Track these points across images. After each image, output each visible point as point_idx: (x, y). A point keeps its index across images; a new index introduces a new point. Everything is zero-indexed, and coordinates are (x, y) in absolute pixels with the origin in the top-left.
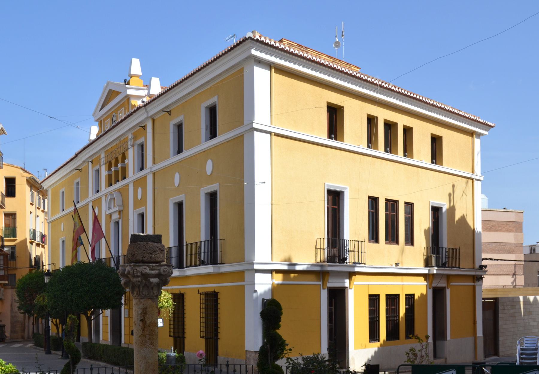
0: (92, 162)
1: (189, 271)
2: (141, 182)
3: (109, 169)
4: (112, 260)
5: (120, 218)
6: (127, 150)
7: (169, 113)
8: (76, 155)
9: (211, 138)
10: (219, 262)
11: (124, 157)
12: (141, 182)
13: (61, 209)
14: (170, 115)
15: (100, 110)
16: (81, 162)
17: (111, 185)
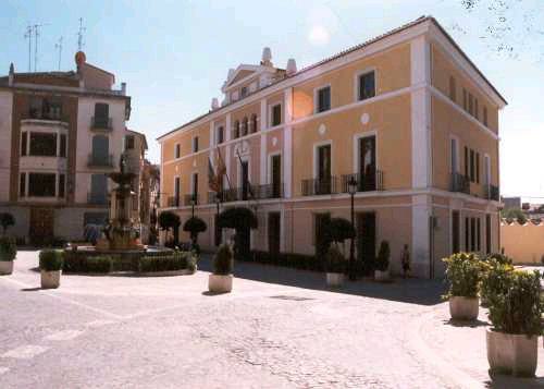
9: (321, 111)
17: (238, 136)
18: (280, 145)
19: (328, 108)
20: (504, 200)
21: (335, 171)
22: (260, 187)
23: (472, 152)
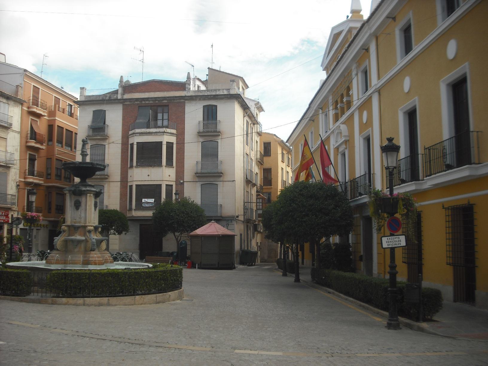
0: (322, 109)
1: (428, 183)
2: (366, 105)
3: (336, 108)
5: (346, 148)
8: (310, 105)
11: (349, 89)
12: (366, 105)
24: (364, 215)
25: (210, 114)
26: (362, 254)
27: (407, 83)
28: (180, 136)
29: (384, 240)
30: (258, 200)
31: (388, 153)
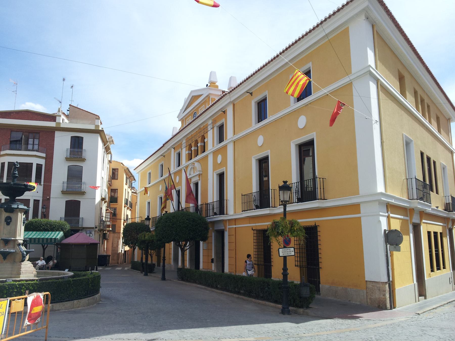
0: (174, 148)
4: (204, 205)
6: (207, 132)
7: (251, 94)
8: (164, 145)
9: (258, 122)
10: (271, 206)
11: (203, 138)
13: (148, 183)
14: (252, 95)
15: (202, 95)
16: (166, 149)
18: (224, 162)
19: (265, 117)
20: (443, 231)
21: (274, 183)
22: (207, 204)
23: (429, 159)
24: (216, 229)
25: (77, 144)
26: (213, 257)
27: (260, 140)
28: (49, 159)
29: (281, 250)
30: (107, 214)
31: (285, 192)
